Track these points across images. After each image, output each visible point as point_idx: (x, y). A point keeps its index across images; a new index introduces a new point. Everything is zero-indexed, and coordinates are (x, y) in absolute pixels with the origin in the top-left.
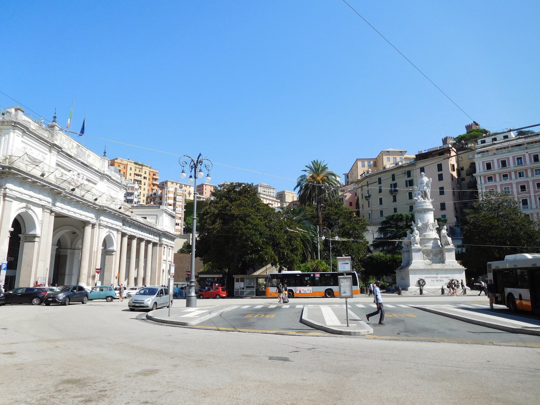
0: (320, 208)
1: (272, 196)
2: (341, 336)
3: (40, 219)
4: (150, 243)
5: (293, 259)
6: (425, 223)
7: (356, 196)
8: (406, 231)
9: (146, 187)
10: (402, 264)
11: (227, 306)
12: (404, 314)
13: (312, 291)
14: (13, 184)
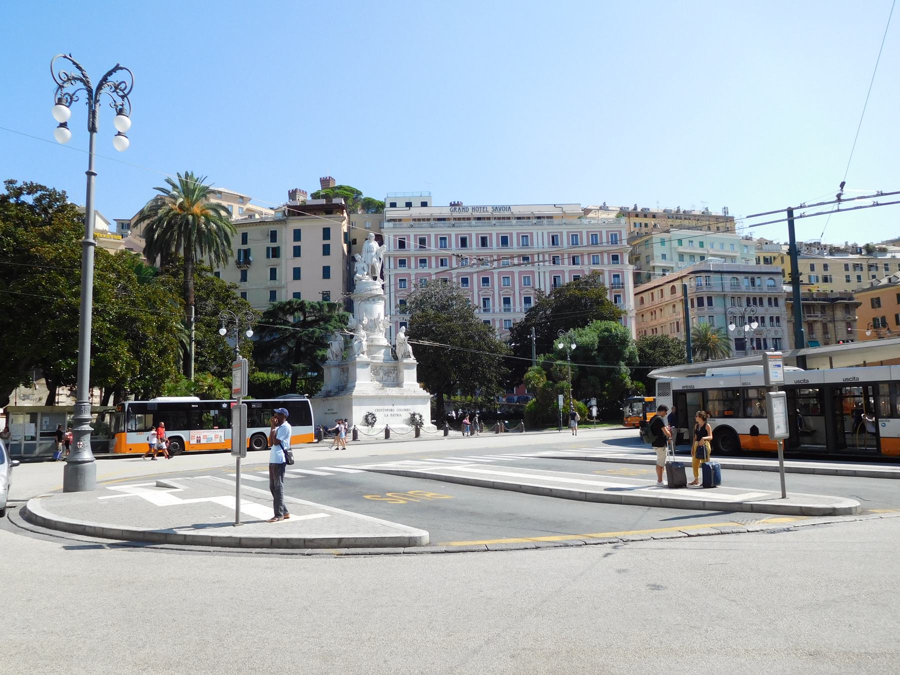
13: (223, 439)
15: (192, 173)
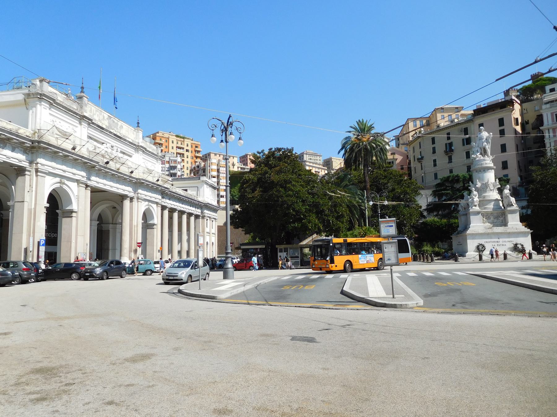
0: (368, 172)
1: (319, 163)
2: (385, 309)
3: (76, 194)
4: (192, 216)
5: (339, 226)
6: (484, 183)
7: (407, 159)
8: (463, 193)
9: (189, 160)
10: (459, 229)
11: (265, 277)
12: (461, 283)
14: (55, 163)
15: (362, 119)
